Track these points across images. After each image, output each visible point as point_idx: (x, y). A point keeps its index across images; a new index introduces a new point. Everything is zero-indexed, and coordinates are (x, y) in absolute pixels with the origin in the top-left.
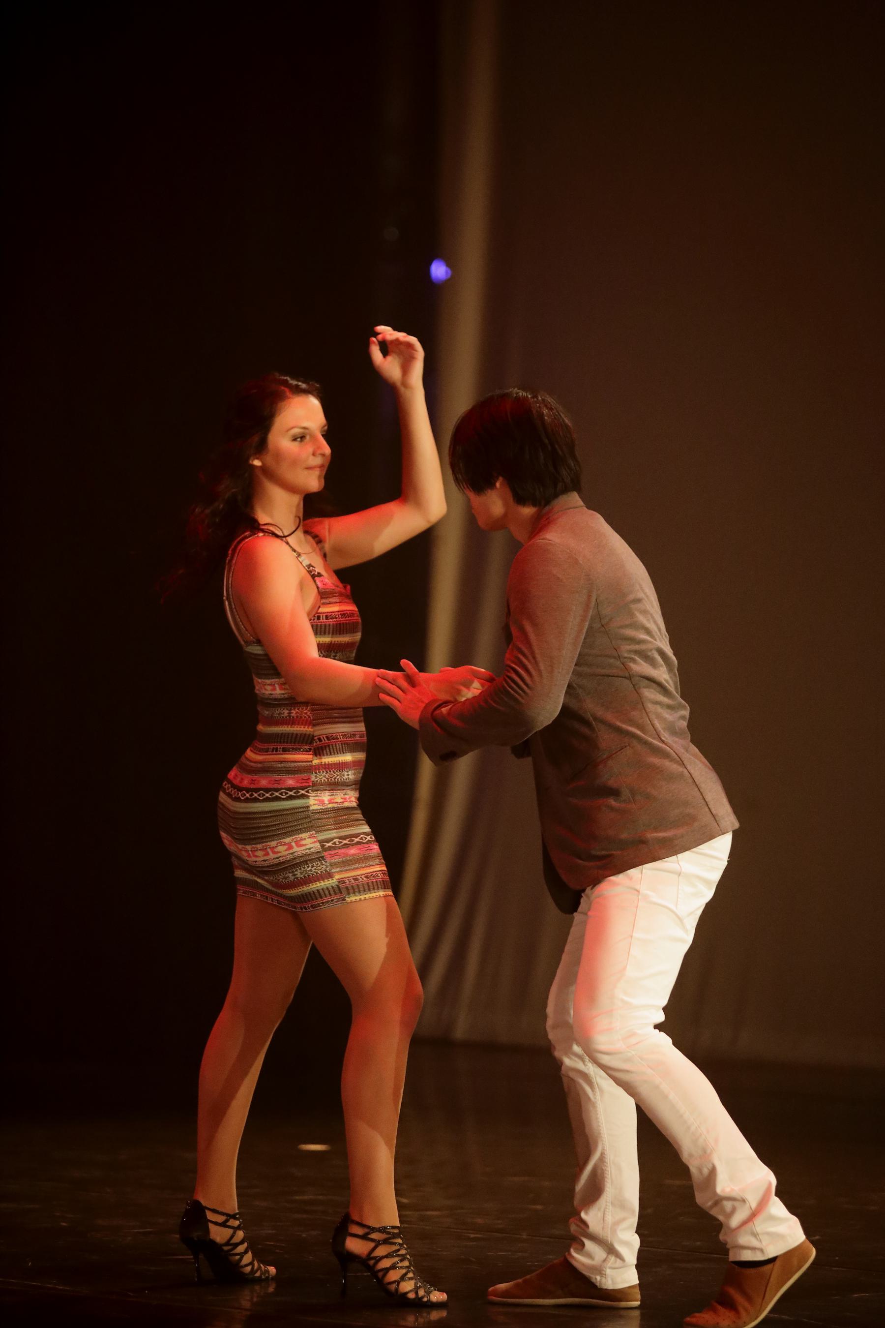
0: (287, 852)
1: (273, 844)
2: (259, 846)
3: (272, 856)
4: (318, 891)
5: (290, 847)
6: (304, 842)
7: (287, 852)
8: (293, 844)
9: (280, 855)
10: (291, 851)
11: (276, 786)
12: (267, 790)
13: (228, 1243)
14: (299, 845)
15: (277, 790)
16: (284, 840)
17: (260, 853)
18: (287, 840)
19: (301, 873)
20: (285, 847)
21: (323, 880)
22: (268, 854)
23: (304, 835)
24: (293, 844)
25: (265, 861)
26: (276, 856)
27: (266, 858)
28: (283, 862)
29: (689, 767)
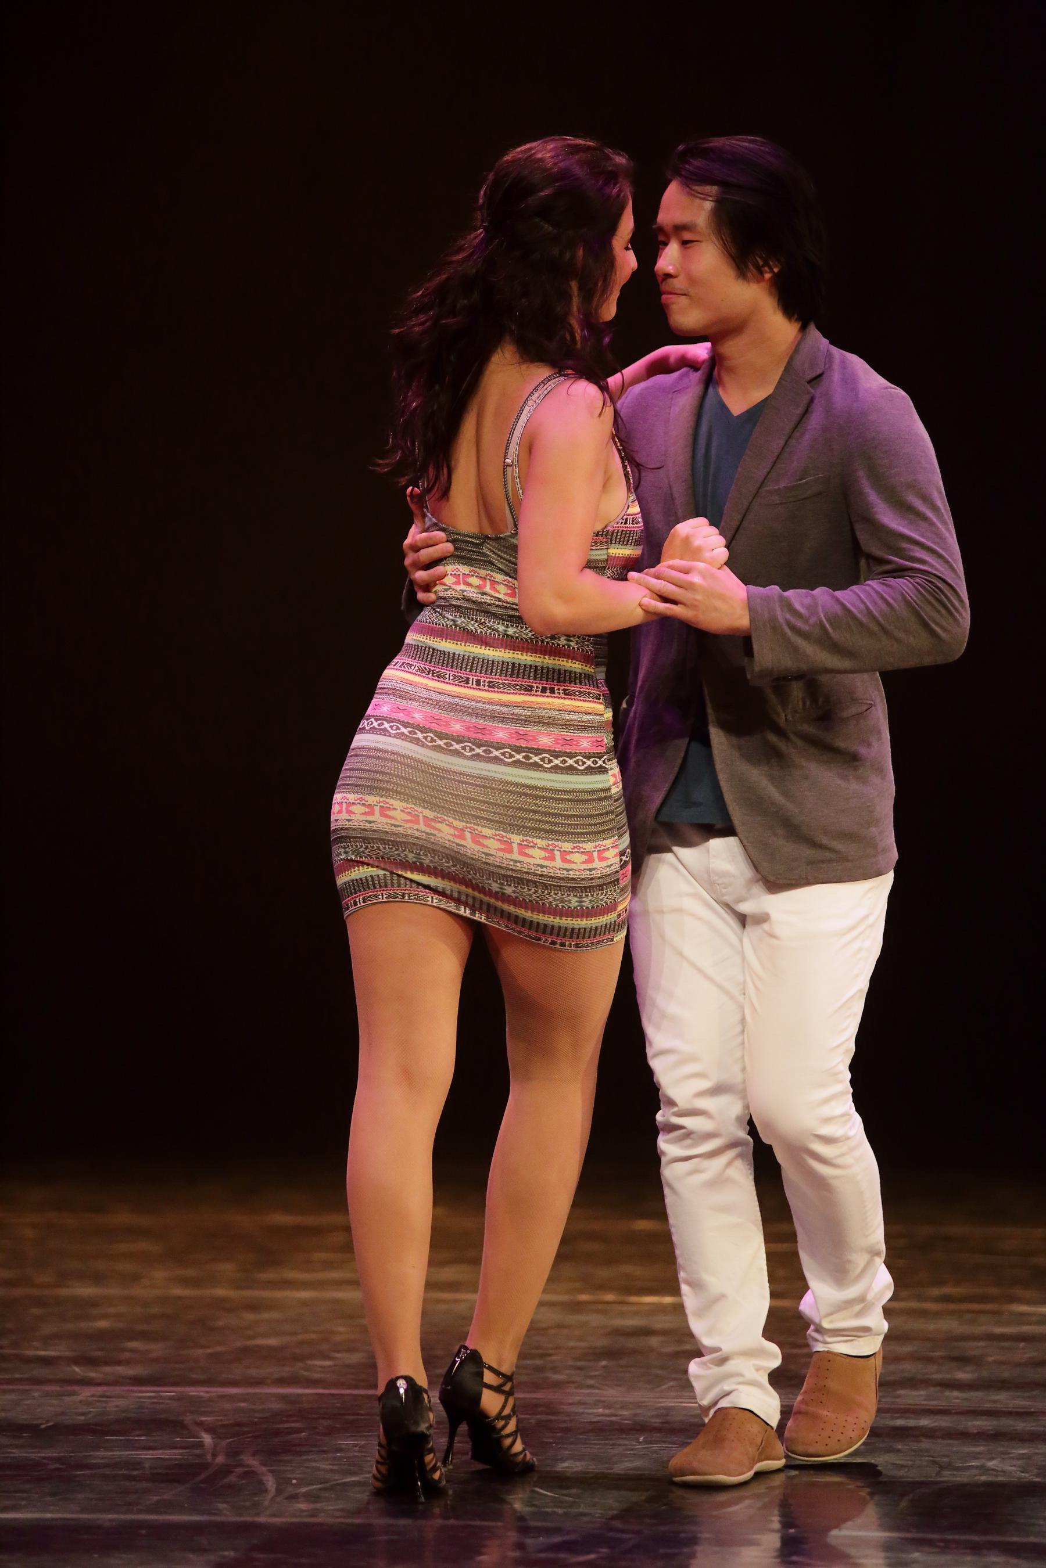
0: (585, 866)
1: (567, 846)
2: (541, 843)
3: (558, 863)
4: (372, 877)
5: (590, 860)
6: (606, 854)
7: (585, 866)
8: (595, 854)
9: (572, 866)
10: (590, 866)
11: (567, 749)
12: (556, 755)
13: (499, 1417)
14: (602, 859)
15: (571, 756)
16: (367, 797)
17: (537, 853)
18: (589, 846)
19: (591, 901)
20: (584, 857)
21: (532, 911)
22: (552, 858)
23: (397, 804)
24: (377, 809)
25: (542, 866)
26: (428, 830)
27: (546, 863)
28: (573, 879)
29: (746, 503)
